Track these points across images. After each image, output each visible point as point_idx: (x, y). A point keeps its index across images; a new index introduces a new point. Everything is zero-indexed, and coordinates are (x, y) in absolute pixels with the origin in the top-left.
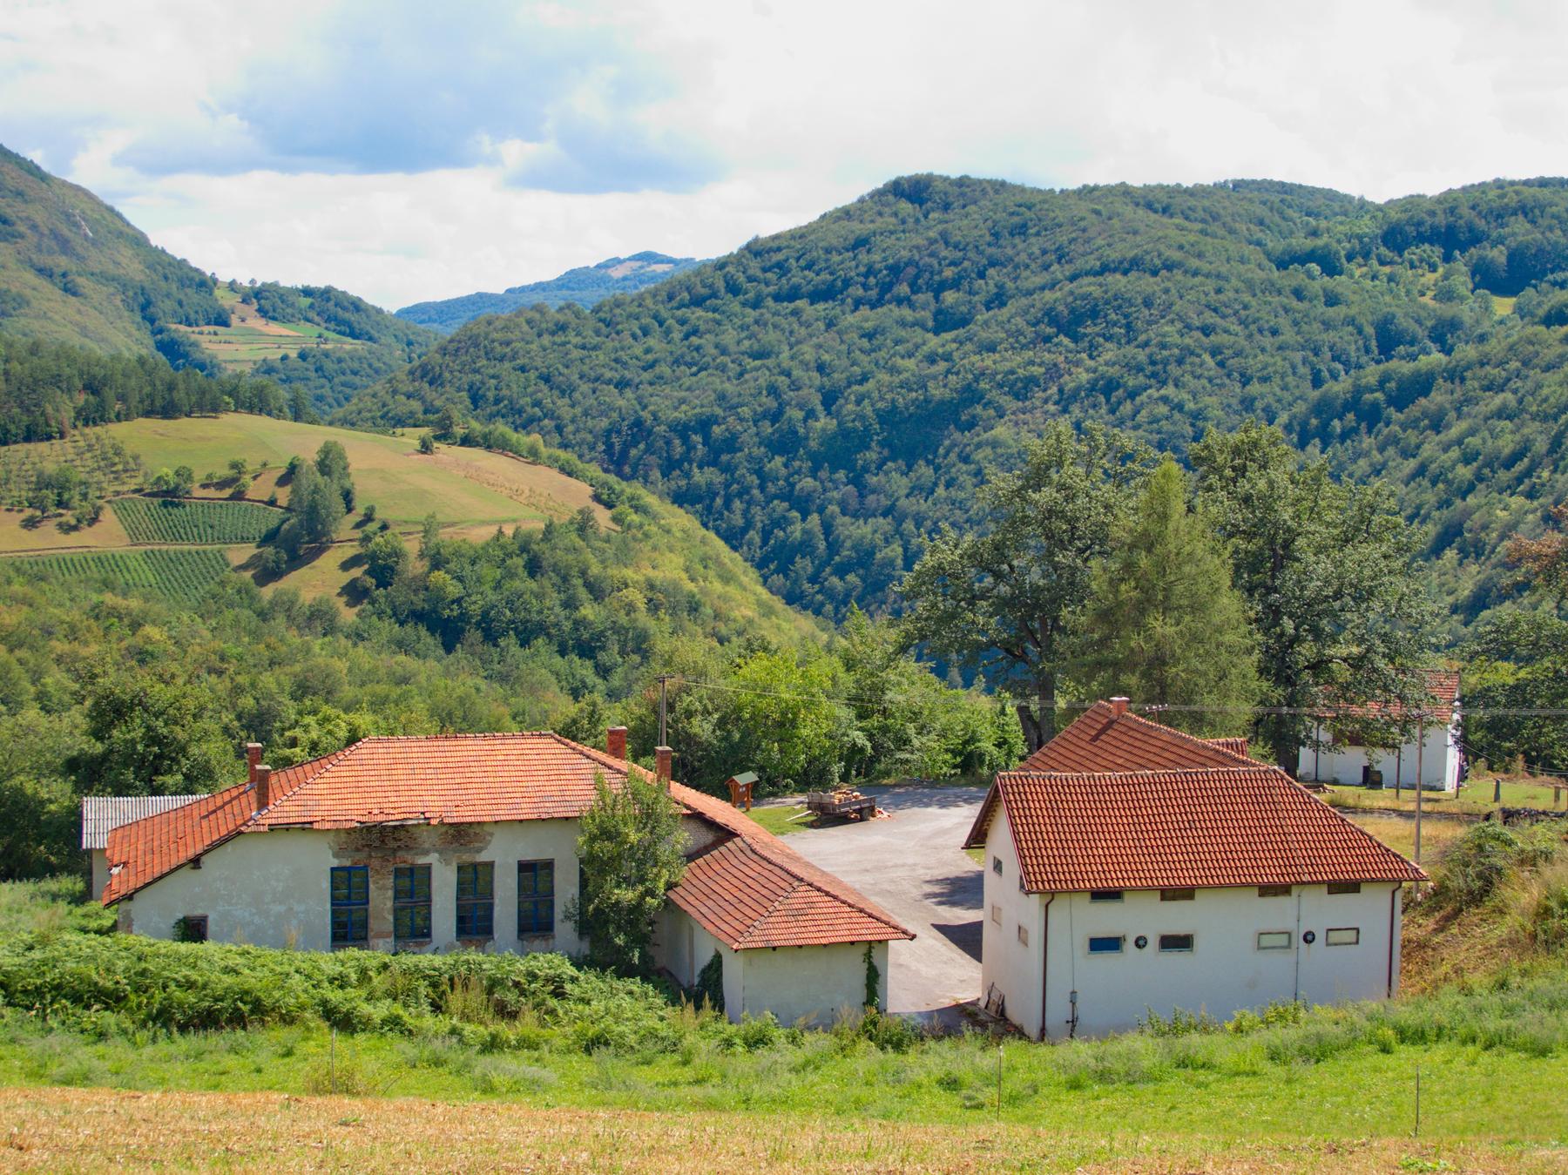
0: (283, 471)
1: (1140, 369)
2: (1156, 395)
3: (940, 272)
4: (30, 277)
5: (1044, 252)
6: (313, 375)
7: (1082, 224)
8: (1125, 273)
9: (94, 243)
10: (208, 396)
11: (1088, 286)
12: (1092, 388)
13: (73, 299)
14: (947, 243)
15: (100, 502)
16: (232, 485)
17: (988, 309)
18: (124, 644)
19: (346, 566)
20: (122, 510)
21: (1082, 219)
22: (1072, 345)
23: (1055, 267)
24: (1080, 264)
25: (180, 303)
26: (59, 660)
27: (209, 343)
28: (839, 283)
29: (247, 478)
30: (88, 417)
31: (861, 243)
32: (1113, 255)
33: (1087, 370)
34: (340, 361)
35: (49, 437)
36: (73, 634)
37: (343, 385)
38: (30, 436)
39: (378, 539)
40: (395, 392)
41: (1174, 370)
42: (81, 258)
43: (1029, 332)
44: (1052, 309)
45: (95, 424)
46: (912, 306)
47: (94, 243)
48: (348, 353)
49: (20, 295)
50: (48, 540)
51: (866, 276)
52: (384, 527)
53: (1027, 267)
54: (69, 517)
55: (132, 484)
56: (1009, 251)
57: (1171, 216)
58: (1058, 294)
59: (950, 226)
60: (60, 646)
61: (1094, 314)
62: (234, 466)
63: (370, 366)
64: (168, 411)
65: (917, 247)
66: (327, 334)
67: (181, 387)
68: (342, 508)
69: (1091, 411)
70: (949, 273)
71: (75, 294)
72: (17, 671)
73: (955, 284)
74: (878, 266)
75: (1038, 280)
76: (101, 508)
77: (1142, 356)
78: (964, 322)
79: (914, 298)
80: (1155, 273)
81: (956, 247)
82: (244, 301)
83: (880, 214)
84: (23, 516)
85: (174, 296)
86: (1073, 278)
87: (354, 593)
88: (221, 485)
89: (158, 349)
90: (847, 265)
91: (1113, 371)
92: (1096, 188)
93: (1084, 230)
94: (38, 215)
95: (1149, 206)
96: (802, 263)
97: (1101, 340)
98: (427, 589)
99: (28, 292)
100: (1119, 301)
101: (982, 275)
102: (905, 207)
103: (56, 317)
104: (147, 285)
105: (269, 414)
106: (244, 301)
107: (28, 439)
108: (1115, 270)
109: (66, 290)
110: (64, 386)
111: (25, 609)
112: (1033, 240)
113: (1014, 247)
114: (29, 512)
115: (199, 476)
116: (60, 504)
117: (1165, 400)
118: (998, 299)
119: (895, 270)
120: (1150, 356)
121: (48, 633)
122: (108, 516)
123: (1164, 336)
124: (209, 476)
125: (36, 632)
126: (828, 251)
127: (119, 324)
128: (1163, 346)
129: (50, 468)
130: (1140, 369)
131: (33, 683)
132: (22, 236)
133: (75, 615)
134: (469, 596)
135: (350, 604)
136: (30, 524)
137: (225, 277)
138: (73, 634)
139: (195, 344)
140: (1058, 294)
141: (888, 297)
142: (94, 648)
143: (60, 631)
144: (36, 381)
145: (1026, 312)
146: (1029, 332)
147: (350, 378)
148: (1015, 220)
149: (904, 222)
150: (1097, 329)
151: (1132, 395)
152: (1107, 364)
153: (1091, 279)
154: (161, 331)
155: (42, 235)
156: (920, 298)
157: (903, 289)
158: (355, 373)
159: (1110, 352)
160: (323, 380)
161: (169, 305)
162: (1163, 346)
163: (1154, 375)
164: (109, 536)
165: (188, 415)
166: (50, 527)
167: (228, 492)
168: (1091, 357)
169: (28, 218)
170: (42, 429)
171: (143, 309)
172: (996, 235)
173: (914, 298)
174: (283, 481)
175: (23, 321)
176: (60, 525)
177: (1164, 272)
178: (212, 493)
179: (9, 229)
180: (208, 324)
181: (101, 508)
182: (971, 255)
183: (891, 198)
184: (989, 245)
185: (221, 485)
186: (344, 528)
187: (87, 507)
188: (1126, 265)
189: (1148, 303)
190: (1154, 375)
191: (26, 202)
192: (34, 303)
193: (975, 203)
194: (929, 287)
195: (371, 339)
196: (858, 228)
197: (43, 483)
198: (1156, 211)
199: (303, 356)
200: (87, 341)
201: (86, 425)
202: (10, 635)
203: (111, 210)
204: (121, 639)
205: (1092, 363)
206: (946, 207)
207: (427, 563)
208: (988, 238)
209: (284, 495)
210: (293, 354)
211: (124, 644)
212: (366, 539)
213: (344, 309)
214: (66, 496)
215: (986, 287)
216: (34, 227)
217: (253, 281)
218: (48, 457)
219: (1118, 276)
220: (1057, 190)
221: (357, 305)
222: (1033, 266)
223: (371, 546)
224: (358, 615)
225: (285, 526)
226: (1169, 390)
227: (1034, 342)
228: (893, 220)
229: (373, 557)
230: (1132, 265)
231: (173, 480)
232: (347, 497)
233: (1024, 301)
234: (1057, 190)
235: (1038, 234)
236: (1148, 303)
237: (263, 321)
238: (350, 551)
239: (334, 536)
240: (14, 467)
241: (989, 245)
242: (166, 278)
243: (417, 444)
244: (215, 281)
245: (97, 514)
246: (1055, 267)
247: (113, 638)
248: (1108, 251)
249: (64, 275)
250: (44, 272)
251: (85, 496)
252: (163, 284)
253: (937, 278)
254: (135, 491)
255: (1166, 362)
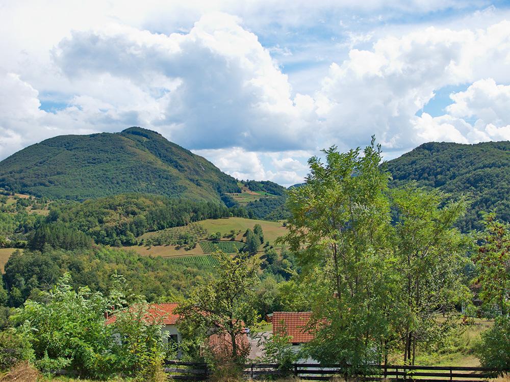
0: (245, 233)
1: (495, 195)
2: (500, 203)
3: (436, 170)
4: (188, 182)
5: (467, 163)
6: (263, 205)
7: (478, 154)
8: (490, 168)
9: (205, 172)
10: (226, 213)
11: (479, 172)
12: (481, 201)
13: (199, 187)
14: (438, 162)
15: (195, 242)
16: (231, 237)
17: (450, 180)
18: (191, 281)
19: (261, 258)
20: (201, 244)
21: (478, 152)
22: (475, 189)
23: (470, 167)
24: (477, 165)
25: (228, 187)
26: (173, 286)
27: (235, 197)
28: (407, 174)
29: (235, 235)
30: (194, 219)
31: (413, 162)
32: (486, 163)
33: (480, 196)
34: (271, 201)
35: (183, 225)
36: (178, 278)
37: (272, 208)
38: (178, 225)
39: (270, 251)
40: (283, 210)
41: (506, 195)
42: (202, 176)
43: (462, 186)
44: (469, 179)
45: (195, 221)
46: (428, 180)
47: (205, 172)
48: (273, 199)
49: (185, 187)
50: (182, 253)
51: (415, 172)
52: (271, 247)
53: (462, 167)
54: (188, 247)
55: (205, 237)
56: (456, 163)
57: (506, 150)
58: (470, 175)
59: (439, 157)
60: (174, 282)
61: (481, 180)
62: (232, 232)
63: (279, 202)
64: (215, 217)
65: (429, 163)
66: (267, 194)
67: (232, 210)
68: (260, 242)
69: (481, 208)
70: (439, 170)
71: (200, 186)
72: (162, 288)
73: (441, 173)
74: (418, 169)
75: (465, 171)
76: (196, 244)
77: (496, 191)
78: (444, 183)
79: (429, 177)
80: (499, 167)
81: (441, 162)
82: (245, 186)
83: (419, 154)
84: (176, 246)
85: (226, 184)
86: (475, 170)
87: (263, 266)
88: (228, 237)
89: (222, 200)
90: (409, 169)
91: (487, 196)
92: (483, 143)
93: (478, 156)
94: (190, 164)
95: (499, 148)
96: (397, 169)
97: (484, 187)
98: (282, 264)
99: (187, 186)
100: (489, 176)
101: (448, 170)
102: (426, 152)
103: (194, 192)
104: (219, 182)
105: (243, 217)
106: (245, 186)
107: (178, 226)
108: (487, 167)
109: (197, 185)
110: (188, 211)
111: (166, 271)
112: (463, 159)
113: (458, 161)
114: (177, 245)
115: (222, 235)
116: (185, 243)
117: (503, 204)
118: (453, 177)
119: (423, 170)
120: (498, 191)
121: (171, 278)
122: (198, 246)
123: (502, 185)
124: (225, 235)
125: (168, 278)
126: (404, 165)
127: (211, 193)
128: (502, 188)
129: (183, 233)
130: (495, 195)
131: (166, 292)
132: (186, 171)
133: (179, 273)
134: (294, 266)
135: (261, 269)
136: (177, 248)
137: (240, 179)
138: (178, 278)
139: (232, 198)
140: (470, 175)
141: (421, 177)
142: (183, 282)
143: (175, 277)
144: (180, 210)
145: (461, 180)
146: (462, 186)
147: (273, 206)
148: (458, 154)
149: (426, 156)
150: (482, 184)
151: (493, 203)
152: (485, 194)
153: (480, 170)
154: (223, 195)
155: (191, 170)
156: (431, 177)
157: (426, 175)
158: (275, 205)
159: (486, 191)
160: (266, 207)
161: (225, 188)
162: (502, 188)
163: (499, 197)
164: (198, 252)
165: (220, 218)
166: (182, 249)
167: (230, 239)
168: (481, 193)
169: (188, 166)
170: (181, 222)
171: (218, 189)
172: (452, 158)
173: (429, 177)
174: (245, 235)
175: (186, 193)
176: (185, 249)
177: (502, 167)
178: (226, 239)
179: (183, 169)
180: (235, 192)
181: (196, 244)
182: (445, 164)
183: (422, 149)
184: (450, 161)
185: (228, 237)
186: (261, 248)
187: (192, 244)
188: (491, 165)
189: (497, 176)
190: (499, 197)
191: (187, 162)
192: (189, 189)
193: (446, 149)
194: (433, 174)
195: (280, 195)
196: (413, 158)
197: (181, 237)
198: (501, 149)
199: (261, 200)
200: (203, 198)
201: (193, 222)
202: (161, 278)
203: (210, 162)
204: (190, 280)
205: (481, 194)
206: (438, 151)
207: (283, 257)
208: (450, 159)
209: (245, 239)
210: (258, 200)
211: (191, 281)
212: (266, 251)
213: (272, 187)
214: (187, 241)
215: (450, 173)
216: (189, 168)
217: (248, 180)
218: (182, 230)
219: (488, 169)
220: (472, 144)
221: (276, 186)
222: (463, 167)
223: (267, 253)
224: (263, 272)
225: (245, 248)
226: (504, 201)
227: (464, 189)
228: (423, 155)
229: (268, 256)
230: (493, 165)
231: (215, 235)
232: (262, 239)
233: (461, 177)
234: (472, 144)
235: (465, 157)
236: (497, 176)
237: (250, 191)
238: (262, 254)
239: (258, 250)
240: (174, 233)
241: (450, 161)
242: (224, 180)
243: (282, 224)
244: (237, 180)
245: (195, 246)
246: (470, 167)
247: (188, 279)
248: (485, 161)
249: (197, 181)
250: (191, 180)
251: (192, 241)
252: (223, 182)
253: (435, 171)
254: (206, 239)
255: (503, 193)
